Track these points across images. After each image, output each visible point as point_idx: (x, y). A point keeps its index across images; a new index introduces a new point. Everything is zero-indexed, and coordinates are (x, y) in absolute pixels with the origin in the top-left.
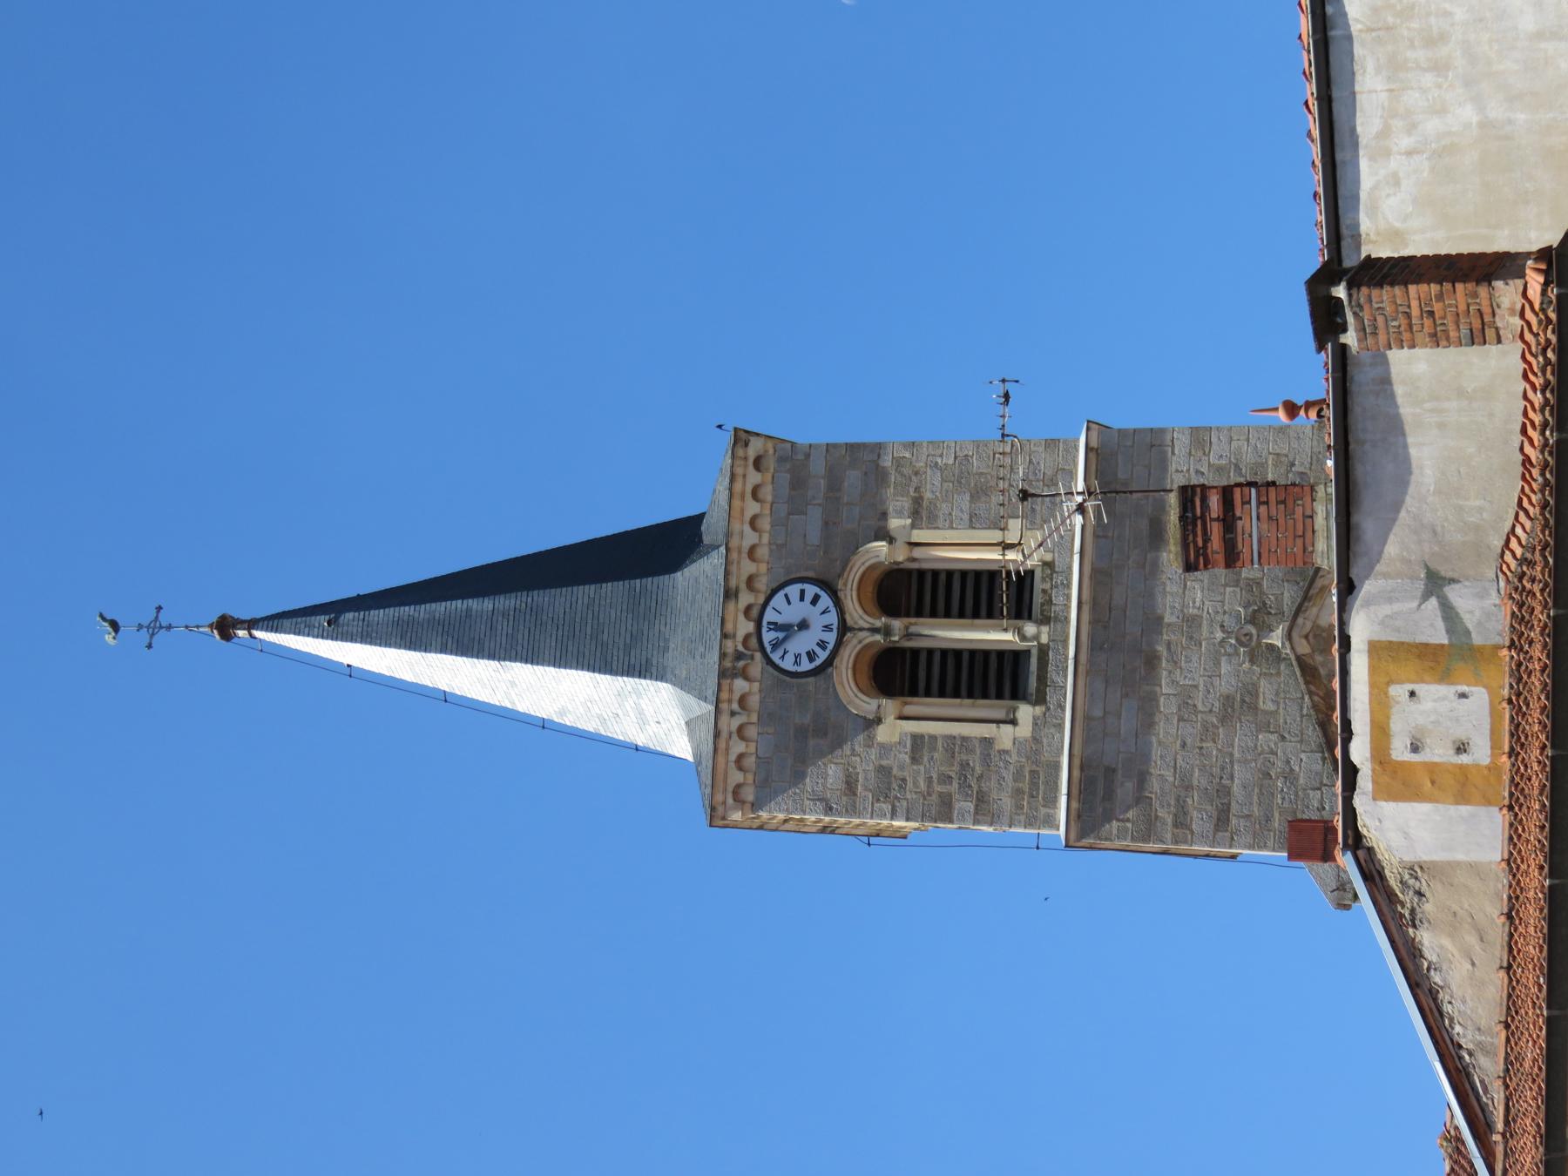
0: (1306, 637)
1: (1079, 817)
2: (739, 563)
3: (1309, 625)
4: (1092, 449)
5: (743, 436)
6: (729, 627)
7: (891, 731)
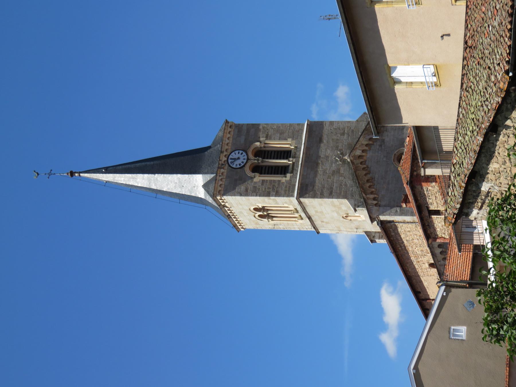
3: (353, 155)
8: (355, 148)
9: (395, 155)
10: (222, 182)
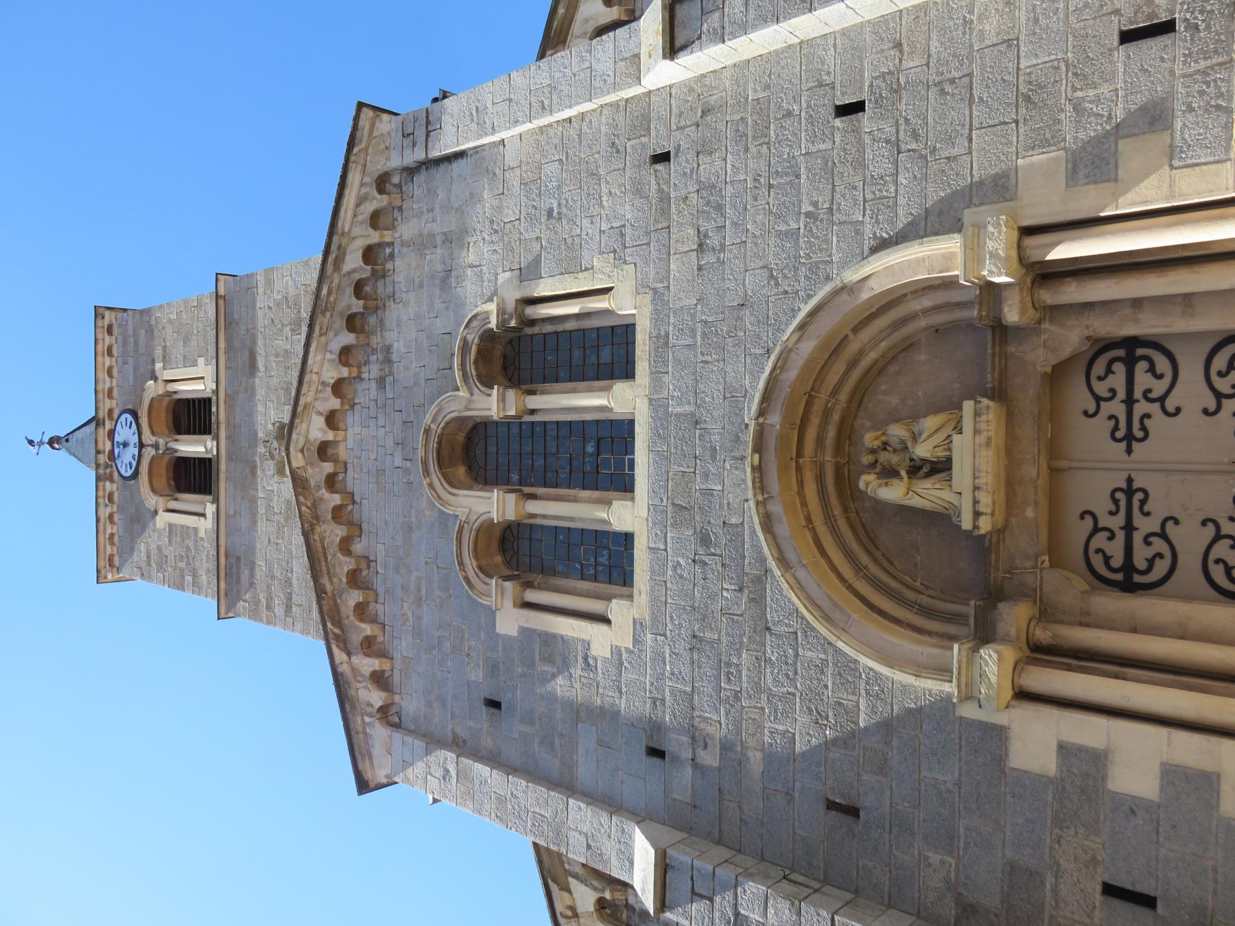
0: (302, 451)
1: (226, 595)
2: (104, 401)
3: (302, 441)
4: (221, 296)
5: (101, 311)
6: (100, 446)
7: (163, 519)
8: (300, 409)
9: (427, 431)
10: (353, 335)
